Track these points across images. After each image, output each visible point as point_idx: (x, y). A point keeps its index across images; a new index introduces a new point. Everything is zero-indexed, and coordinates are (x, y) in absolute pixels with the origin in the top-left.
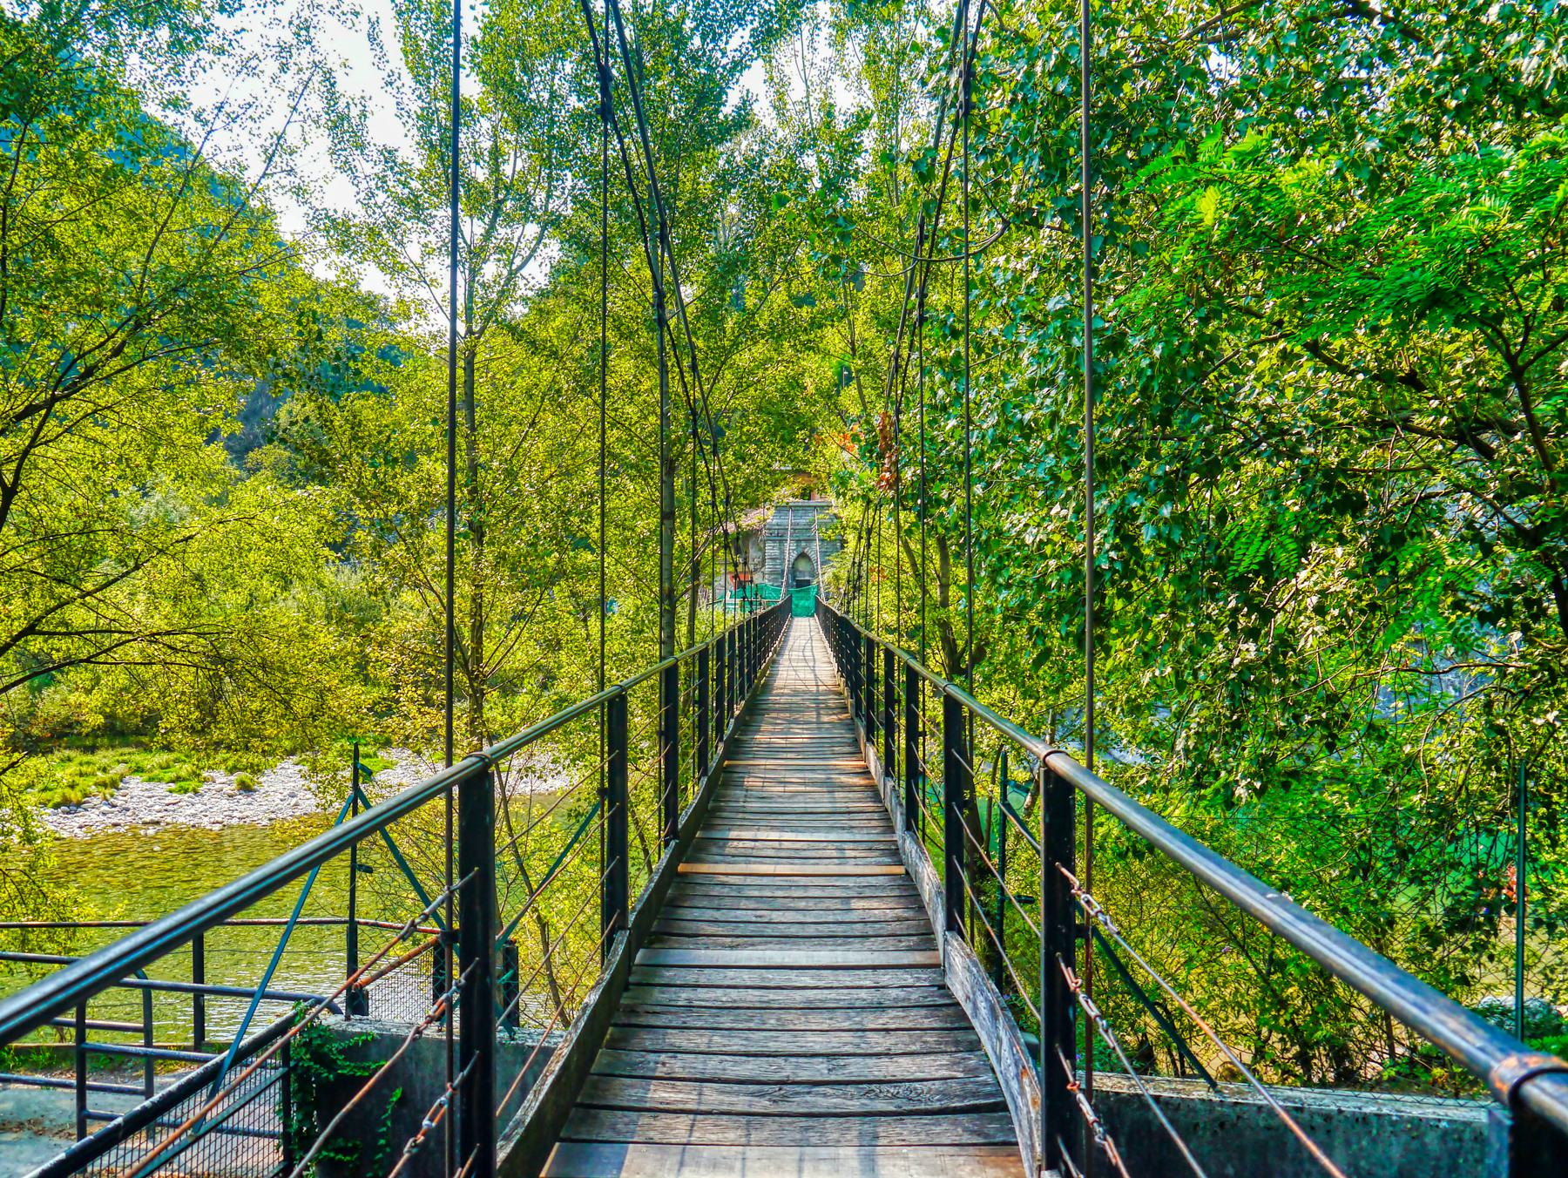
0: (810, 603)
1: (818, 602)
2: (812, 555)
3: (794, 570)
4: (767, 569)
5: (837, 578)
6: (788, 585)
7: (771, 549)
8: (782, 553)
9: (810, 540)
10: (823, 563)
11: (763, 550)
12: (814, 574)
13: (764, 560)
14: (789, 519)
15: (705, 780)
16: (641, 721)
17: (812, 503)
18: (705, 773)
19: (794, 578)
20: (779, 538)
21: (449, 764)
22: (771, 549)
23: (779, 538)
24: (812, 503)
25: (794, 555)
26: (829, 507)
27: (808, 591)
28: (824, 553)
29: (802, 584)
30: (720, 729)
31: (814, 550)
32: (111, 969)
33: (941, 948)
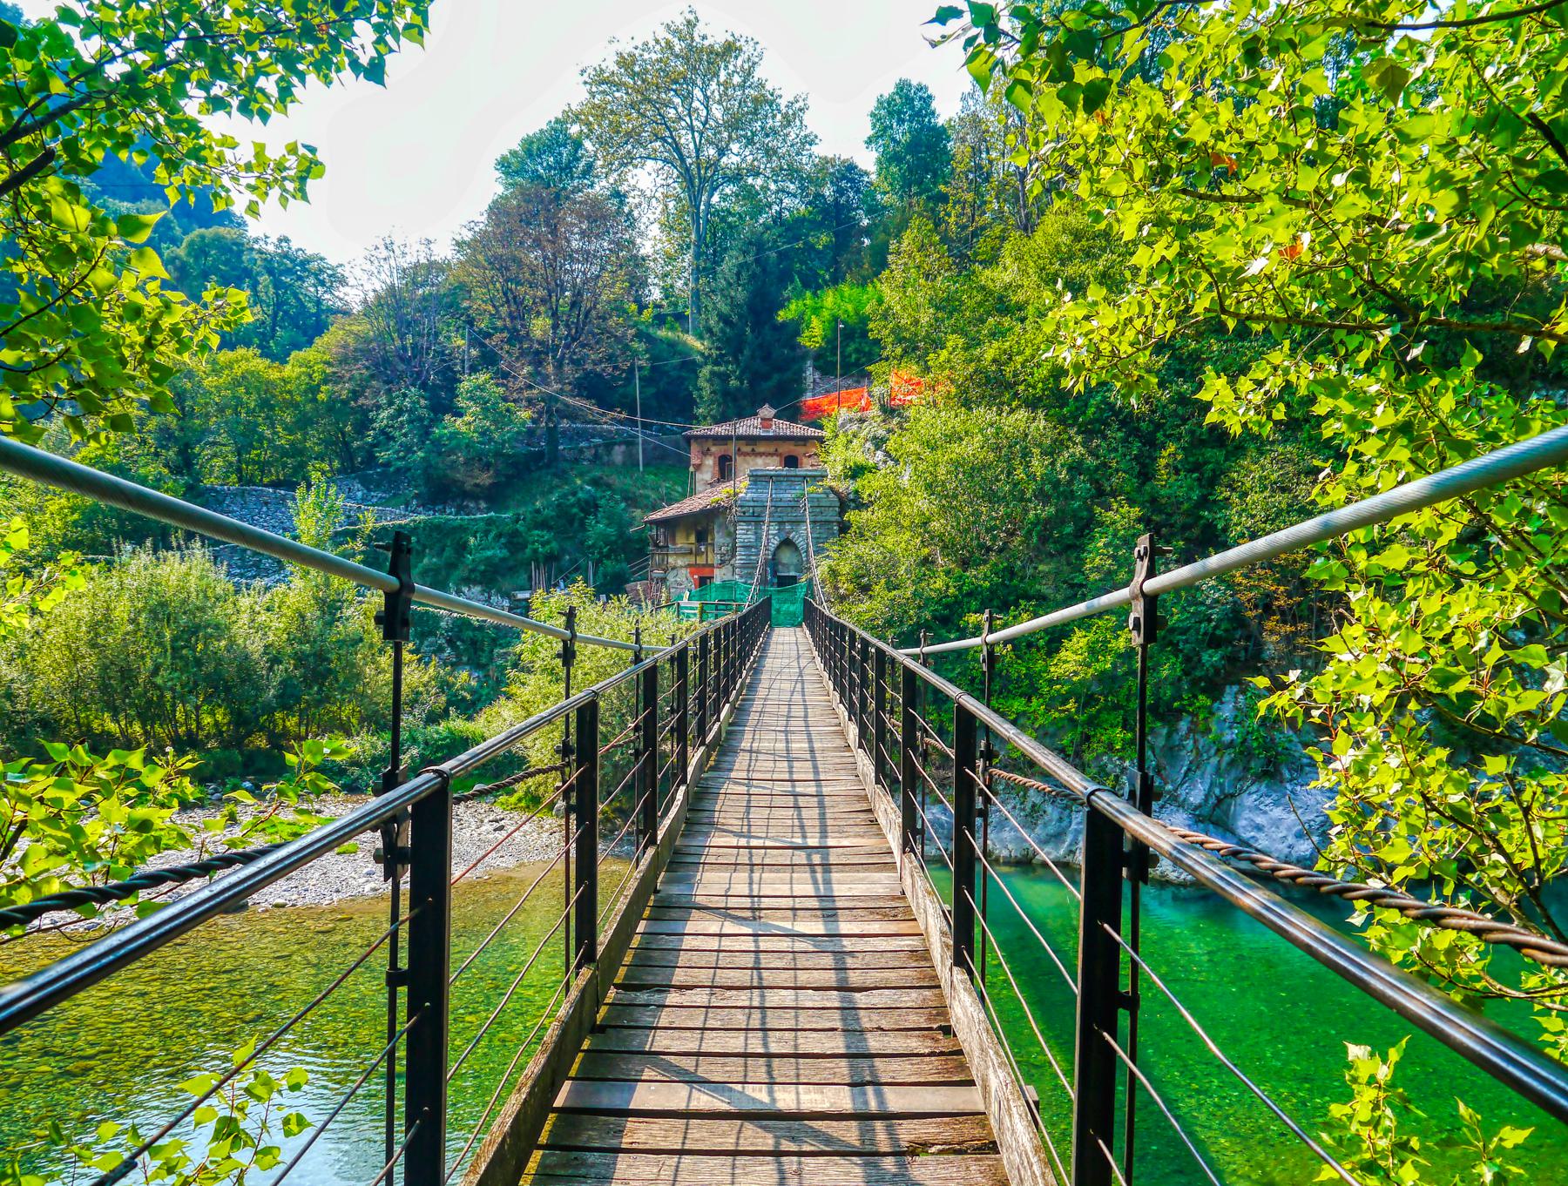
0: (797, 608)
1: (808, 607)
2: (800, 543)
3: (774, 563)
4: (738, 561)
5: (834, 573)
6: (763, 582)
7: (744, 534)
8: (759, 538)
9: (798, 522)
10: (817, 553)
11: (732, 535)
12: (804, 567)
13: (734, 549)
14: (767, 494)
15: (586, 972)
16: (693, 668)
17: (800, 471)
18: (588, 957)
19: (775, 573)
20: (756, 520)
21: (567, 697)
22: (744, 534)
23: (756, 520)
24: (800, 471)
25: (775, 542)
26: (824, 477)
27: (794, 591)
28: (817, 540)
29: (786, 582)
30: (702, 730)
31: (804, 534)
32: (86, 970)
33: (721, 430)
